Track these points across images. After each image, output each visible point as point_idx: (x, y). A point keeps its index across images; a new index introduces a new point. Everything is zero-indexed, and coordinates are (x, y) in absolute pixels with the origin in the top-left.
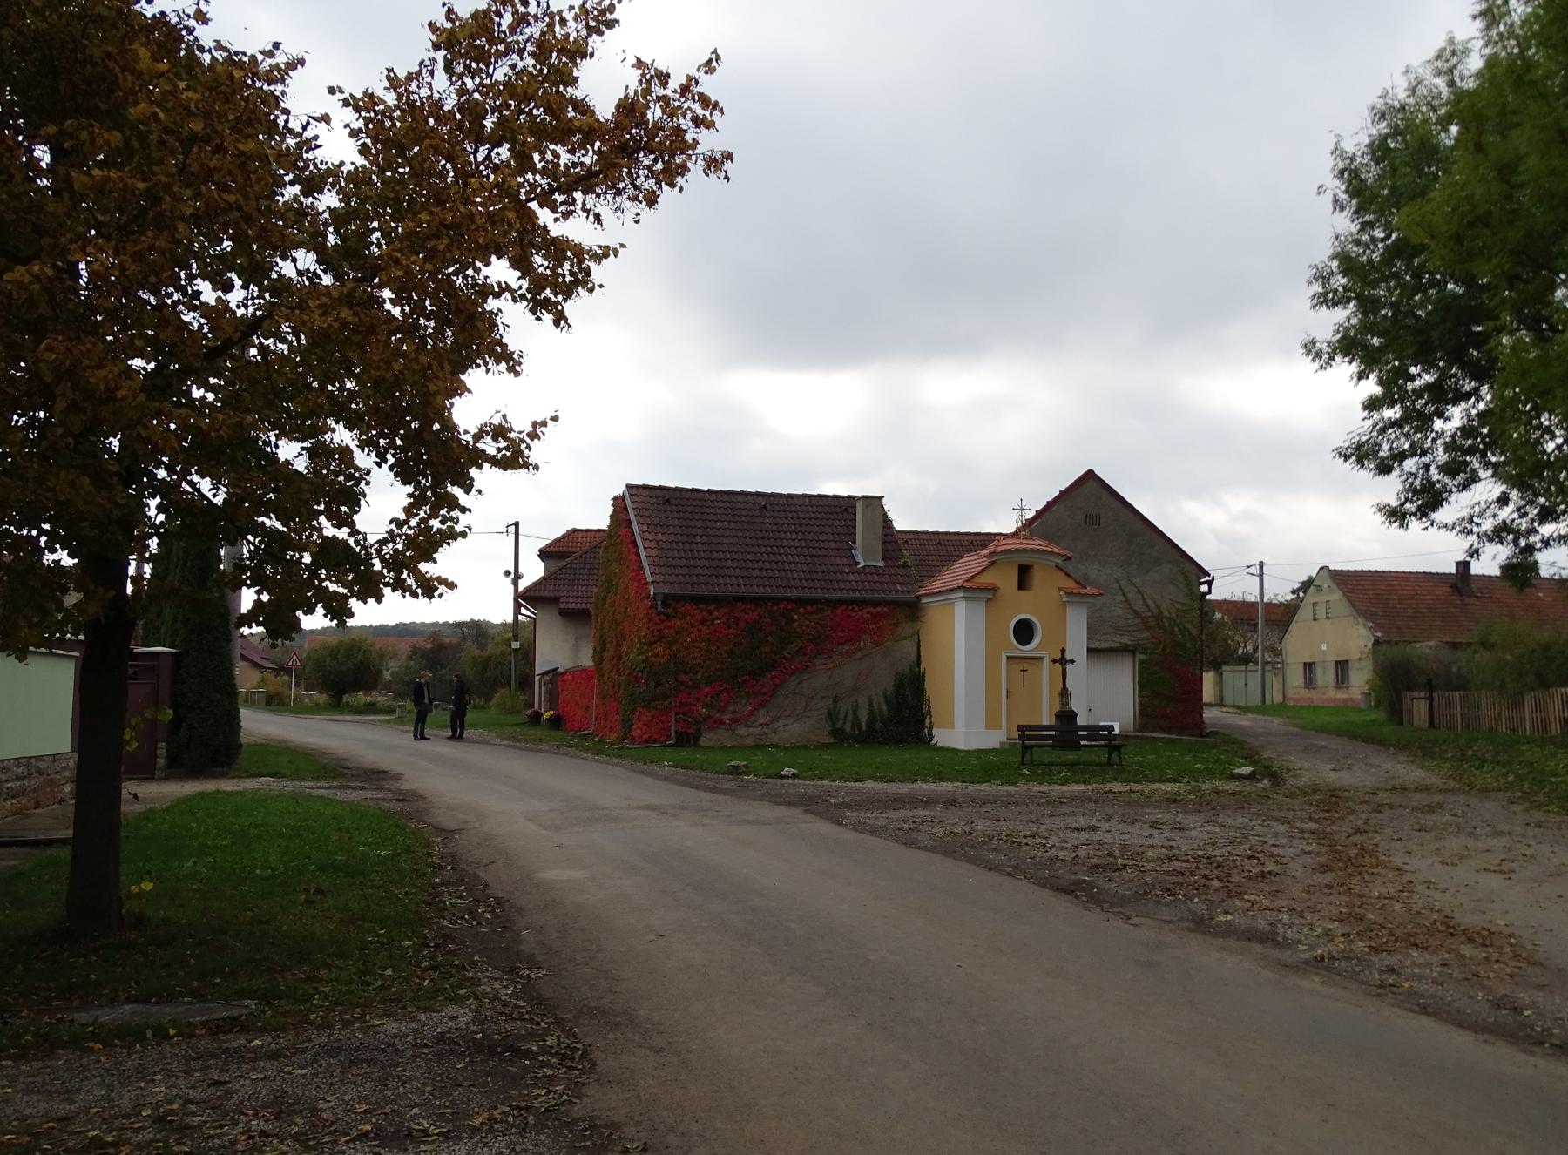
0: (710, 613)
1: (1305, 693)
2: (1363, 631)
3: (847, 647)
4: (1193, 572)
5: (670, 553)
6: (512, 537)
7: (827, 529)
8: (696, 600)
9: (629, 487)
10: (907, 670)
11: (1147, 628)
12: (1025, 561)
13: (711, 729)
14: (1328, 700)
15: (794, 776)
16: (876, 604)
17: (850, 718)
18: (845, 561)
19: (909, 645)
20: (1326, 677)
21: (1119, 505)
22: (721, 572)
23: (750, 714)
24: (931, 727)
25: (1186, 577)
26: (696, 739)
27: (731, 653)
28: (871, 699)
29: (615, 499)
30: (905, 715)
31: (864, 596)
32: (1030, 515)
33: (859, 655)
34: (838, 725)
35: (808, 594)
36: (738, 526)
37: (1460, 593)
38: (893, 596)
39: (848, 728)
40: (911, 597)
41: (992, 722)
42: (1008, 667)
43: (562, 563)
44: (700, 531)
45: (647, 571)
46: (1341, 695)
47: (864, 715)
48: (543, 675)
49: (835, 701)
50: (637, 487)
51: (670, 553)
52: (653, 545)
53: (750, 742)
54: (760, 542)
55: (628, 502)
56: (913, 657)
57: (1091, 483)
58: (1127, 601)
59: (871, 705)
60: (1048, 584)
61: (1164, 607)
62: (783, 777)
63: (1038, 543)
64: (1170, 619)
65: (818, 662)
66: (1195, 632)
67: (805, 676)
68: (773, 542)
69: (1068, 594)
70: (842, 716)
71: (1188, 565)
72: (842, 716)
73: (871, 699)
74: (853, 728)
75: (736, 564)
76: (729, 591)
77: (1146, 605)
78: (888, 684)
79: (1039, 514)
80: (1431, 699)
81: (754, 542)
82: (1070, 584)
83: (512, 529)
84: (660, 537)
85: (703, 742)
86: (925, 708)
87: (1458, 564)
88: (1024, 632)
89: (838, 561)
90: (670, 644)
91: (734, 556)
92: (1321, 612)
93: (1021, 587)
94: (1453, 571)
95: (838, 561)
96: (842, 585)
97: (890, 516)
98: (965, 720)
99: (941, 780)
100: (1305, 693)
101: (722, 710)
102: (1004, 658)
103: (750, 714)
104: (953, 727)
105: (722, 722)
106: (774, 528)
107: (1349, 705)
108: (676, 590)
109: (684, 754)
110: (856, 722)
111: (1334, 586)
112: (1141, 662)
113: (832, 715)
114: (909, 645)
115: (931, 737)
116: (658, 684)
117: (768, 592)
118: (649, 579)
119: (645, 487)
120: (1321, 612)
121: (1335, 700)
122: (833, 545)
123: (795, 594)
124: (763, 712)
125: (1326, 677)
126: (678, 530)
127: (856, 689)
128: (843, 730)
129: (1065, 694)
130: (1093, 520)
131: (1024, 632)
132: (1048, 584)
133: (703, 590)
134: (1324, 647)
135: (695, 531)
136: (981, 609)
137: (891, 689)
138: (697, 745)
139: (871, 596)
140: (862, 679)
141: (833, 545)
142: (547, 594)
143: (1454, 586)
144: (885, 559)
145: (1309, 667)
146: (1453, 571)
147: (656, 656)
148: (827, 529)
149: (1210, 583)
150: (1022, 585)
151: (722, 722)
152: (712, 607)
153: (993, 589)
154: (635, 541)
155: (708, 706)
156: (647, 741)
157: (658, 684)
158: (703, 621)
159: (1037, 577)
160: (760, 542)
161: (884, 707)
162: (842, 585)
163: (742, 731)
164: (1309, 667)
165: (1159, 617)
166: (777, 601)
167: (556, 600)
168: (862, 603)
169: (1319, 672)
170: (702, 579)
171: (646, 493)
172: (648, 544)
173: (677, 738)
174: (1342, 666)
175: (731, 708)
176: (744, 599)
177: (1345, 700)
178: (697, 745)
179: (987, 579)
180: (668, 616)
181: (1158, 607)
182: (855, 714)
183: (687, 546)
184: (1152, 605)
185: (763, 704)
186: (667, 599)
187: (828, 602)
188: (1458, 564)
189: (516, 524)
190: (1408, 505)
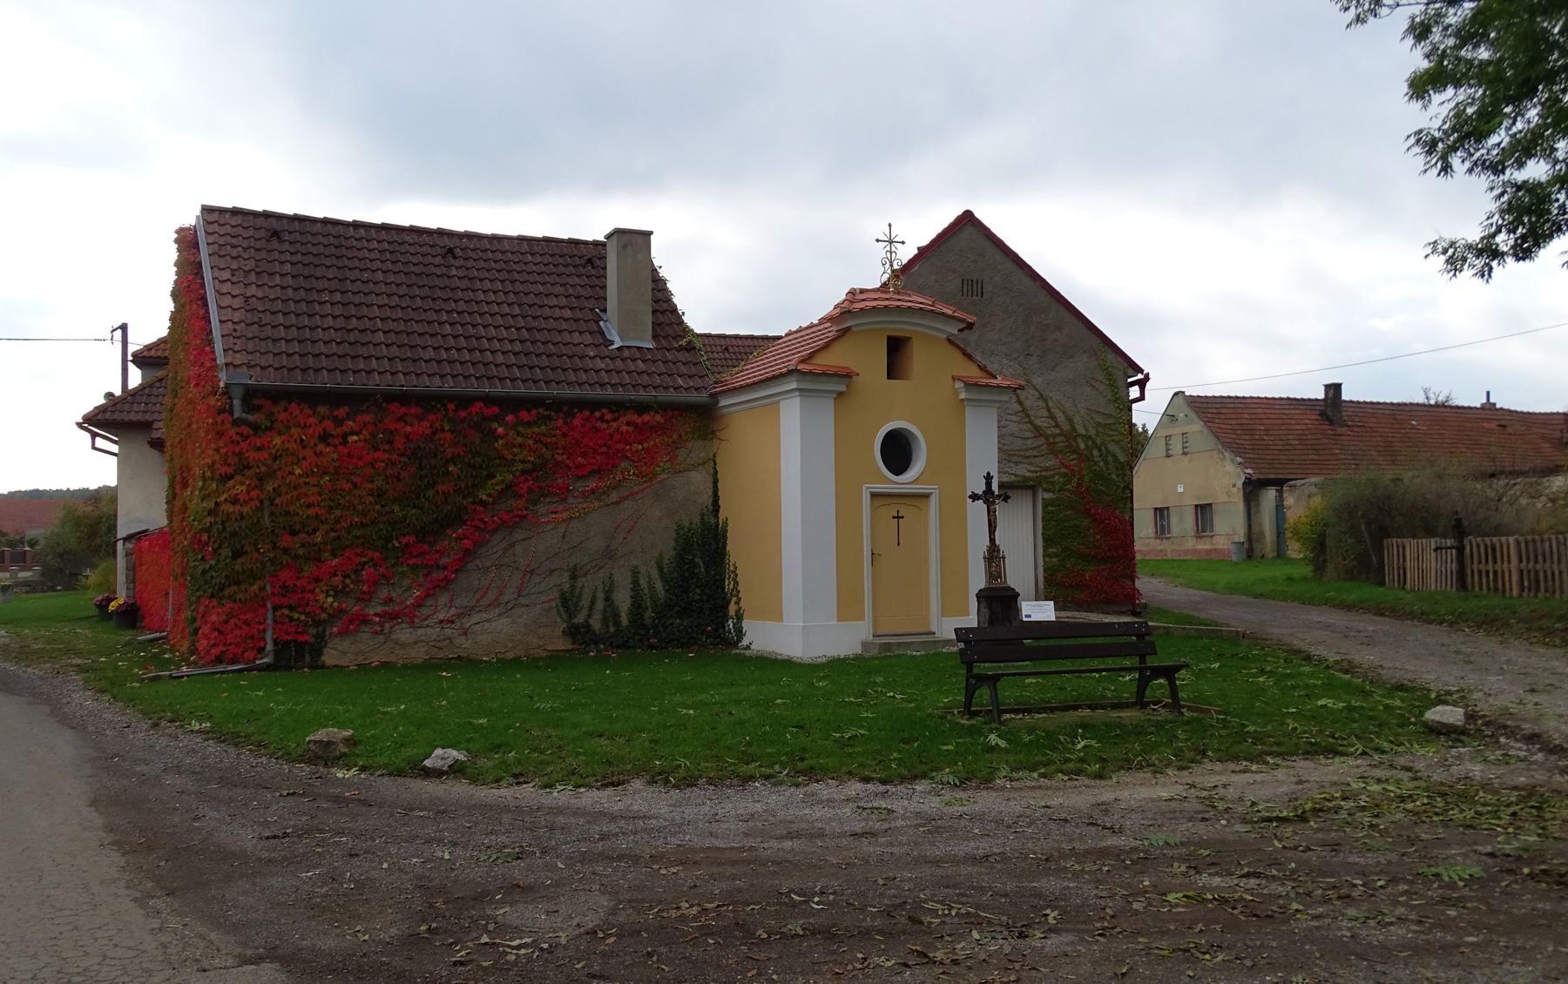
0: (338, 422)
1: (1156, 545)
2: (1230, 468)
3: (591, 483)
4: (1118, 371)
5: (267, 318)
6: (119, 346)
7: (558, 290)
8: (310, 397)
9: (207, 210)
10: (697, 520)
11: (1055, 453)
12: (900, 328)
13: (343, 633)
14: (1187, 552)
15: (456, 770)
16: (641, 408)
17: (600, 605)
18: (588, 339)
19: (699, 479)
20: (1182, 524)
21: (1009, 265)
22: (363, 351)
23: (418, 604)
24: (739, 617)
25: (1110, 376)
26: (317, 652)
27: (380, 494)
28: (635, 573)
29: (180, 231)
30: (696, 598)
31: (620, 394)
32: (906, 253)
33: (614, 496)
34: (580, 618)
35: (522, 390)
36: (401, 278)
37: (1331, 423)
38: (671, 396)
39: (596, 624)
40: (702, 397)
41: (847, 609)
42: (873, 510)
43: (160, 373)
44: (333, 285)
45: (219, 347)
46: (1204, 545)
47: (623, 600)
48: (125, 539)
49: (574, 577)
50: (222, 211)
51: (267, 318)
52: (238, 303)
53: (419, 654)
54: (439, 304)
55: (201, 235)
56: (706, 499)
57: (969, 230)
58: (1024, 411)
59: (635, 582)
60: (934, 366)
61: (1077, 419)
62: (428, 773)
63: (918, 300)
64: (1087, 438)
65: (542, 509)
66: (1122, 458)
67: (519, 535)
68: (461, 306)
69: (970, 385)
70: (585, 602)
71: (1111, 357)
72: (585, 602)
73: (635, 573)
74: (605, 621)
75: (392, 338)
76: (376, 382)
77: (1052, 417)
78: (666, 546)
79: (923, 251)
80: (1460, 550)
81: (428, 304)
82: (972, 371)
83: (119, 333)
84: (252, 290)
85: (329, 657)
86: (728, 585)
87: (1327, 387)
88: (897, 451)
89: (576, 338)
90: (261, 478)
91: (390, 325)
92: (1177, 447)
93: (891, 374)
94: (1322, 396)
95: (576, 338)
96: (583, 377)
97: (663, 273)
98: (799, 611)
99: (813, 774)
100: (1156, 545)
101: (366, 597)
102: (866, 498)
103: (418, 604)
104: (779, 617)
105: (365, 620)
106: (465, 283)
107: (1213, 559)
108: (271, 380)
109: (273, 698)
110: (611, 614)
111: (1194, 416)
112: (1046, 504)
113: (568, 602)
114: (698, 479)
115: (740, 633)
116: (237, 554)
117: (448, 386)
118: (221, 360)
119: (236, 212)
120: (1177, 447)
121: (1195, 552)
122: (567, 313)
123: (498, 389)
124: (443, 599)
125: (1182, 524)
126: (289, 280)
127: (609, 554)
128: (588, 626)
129: (994, 555)
130: (972, 288)
131: (897, 451)
132: (934, 366)
133: (324, 381)
134: (1180, 490)
135: (320, 284)
136: (826, 411)
137: (669, 554)
138: (317, 665)
139: (633, 395)
140: (614, 539)
141: (567, 313)
142: (132, 417)
143: (1323, 414)
144: (655, 337)
145: (1161, 513)
146: (1322, 396)
147: (235, 501)
148: (558, 290)
149: (1142, 384)
150: (893, 371)
151: (365, 620)
152: (342, 411)
153: (847, 376)
154: (204, 299)
155: (338, 592)
156: (219, 660)
157: (237, 554)
158: (324, 438)
159: (920, 357)
160: (439, 304)
161: (659, 585)
162: (583, 377)
163: (404, 634)
164: (1161, 513)
165: (1071, 436)
166: (464, 401)
167: (146, 426)
168: (618, 407)
169: (1174, 520)
170: (324, 362)
171: (237, 220)
172: (226, 301)
173: (277, 653)
174: (1204, 512)
175: (383, 593)
176: (403, 398)
177: (1209, 552)
178: (317, 665)
179: (834, 359)
180: (255, 427)
181: (1070, 421)
182: (607, 599)
183: (303, 307)
184: (1061, 418)
185: (444, 585)
186: (252, 396)
187: (558, 405)
188: (1327, 387)
189: (124, 328)
190: (1500, 238)
